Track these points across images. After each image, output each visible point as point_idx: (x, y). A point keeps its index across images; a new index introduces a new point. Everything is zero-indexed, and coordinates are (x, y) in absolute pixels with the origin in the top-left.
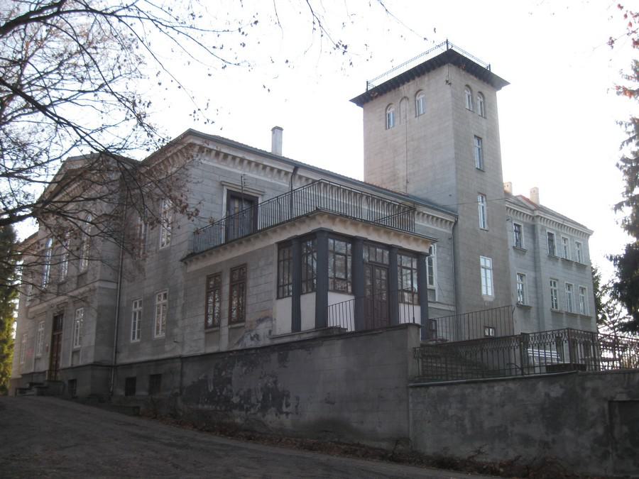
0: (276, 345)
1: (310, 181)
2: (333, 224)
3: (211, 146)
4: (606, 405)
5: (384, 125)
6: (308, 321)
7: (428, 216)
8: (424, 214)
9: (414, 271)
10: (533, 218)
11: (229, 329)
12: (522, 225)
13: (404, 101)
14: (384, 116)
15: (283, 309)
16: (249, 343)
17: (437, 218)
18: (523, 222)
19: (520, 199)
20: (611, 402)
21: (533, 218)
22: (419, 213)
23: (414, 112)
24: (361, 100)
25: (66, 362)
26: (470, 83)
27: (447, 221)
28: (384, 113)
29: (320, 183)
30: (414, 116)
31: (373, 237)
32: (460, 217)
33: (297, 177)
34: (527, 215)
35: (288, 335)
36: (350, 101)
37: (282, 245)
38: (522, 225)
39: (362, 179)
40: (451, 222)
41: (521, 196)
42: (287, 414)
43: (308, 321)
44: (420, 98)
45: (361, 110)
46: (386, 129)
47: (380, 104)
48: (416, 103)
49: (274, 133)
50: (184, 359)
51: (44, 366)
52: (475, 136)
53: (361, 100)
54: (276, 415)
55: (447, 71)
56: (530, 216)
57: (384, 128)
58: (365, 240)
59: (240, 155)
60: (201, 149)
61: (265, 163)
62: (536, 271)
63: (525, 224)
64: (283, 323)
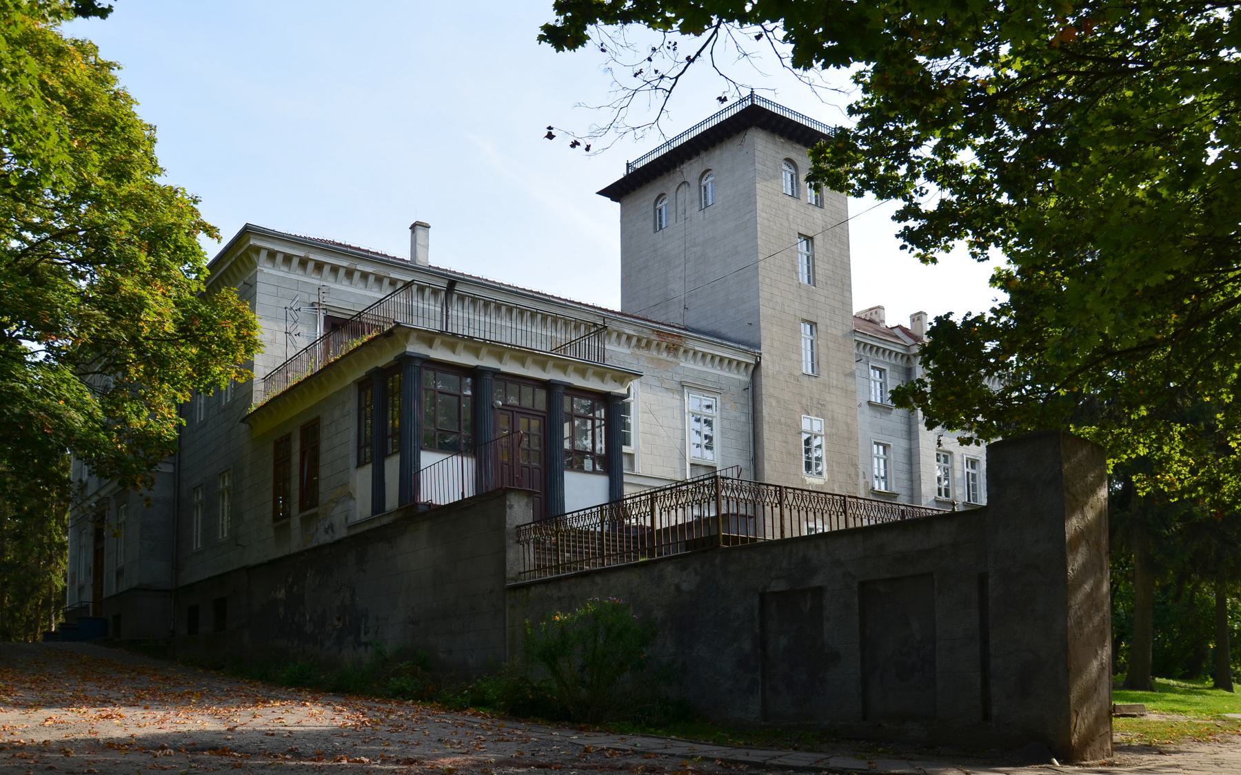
0: (355, 536)
1: (400, 285)
2: (431, 347)
3: (394, 275)
4: (756, 601)
5: (652, 225)
6: (392, 499)
7: (704, 355)
8: (695, 353)
9: (597, 423)
10: (909, 359)
11: (301, 519)
12: (888, 369)
13: (683, 187)
14: (652, 213)
15: (362, 480)
16: (324, 538)
17: (722, 359)
18: (887, 363)
19: (897, 332)
20: (763, 596)
21: (909, 359)
22: (686, 352)
23: (697, 203)
24: (614, 192)
25: (111, 588)
26: (793, 156)
27: (739, 363)
28: (652, 207)
29: (408, 285)
30: (697, 209)
31: (577, 381)
32: (765, 356)
33: (455, 297)
34: (897, 353)
35: (368, 521)
36: (603, 193)
37: (362, 385)
38: (888, 369)
39: (618, 308)
40: (747, 365)
41: (899, 327)
42: (366, 644)
43: (392, 499)
44: (707, 181)
45: (617, 206)
46: (655, 231)
47: (645, 199)
48: (703, 190)
49: (413, 232)
50: (248, 570)
51: (88, 596)
52: (800, 235)
53: (614, 192)
54: (354, 649)
55: (760, 144)
56: (903, 355)
57: (652, 230)
58: (496, 373)
59: (345, 263)
60: (272, 255)
61: (392, 275)
62: (910, 440)
63: (894, 367)
64: (362, 507)
